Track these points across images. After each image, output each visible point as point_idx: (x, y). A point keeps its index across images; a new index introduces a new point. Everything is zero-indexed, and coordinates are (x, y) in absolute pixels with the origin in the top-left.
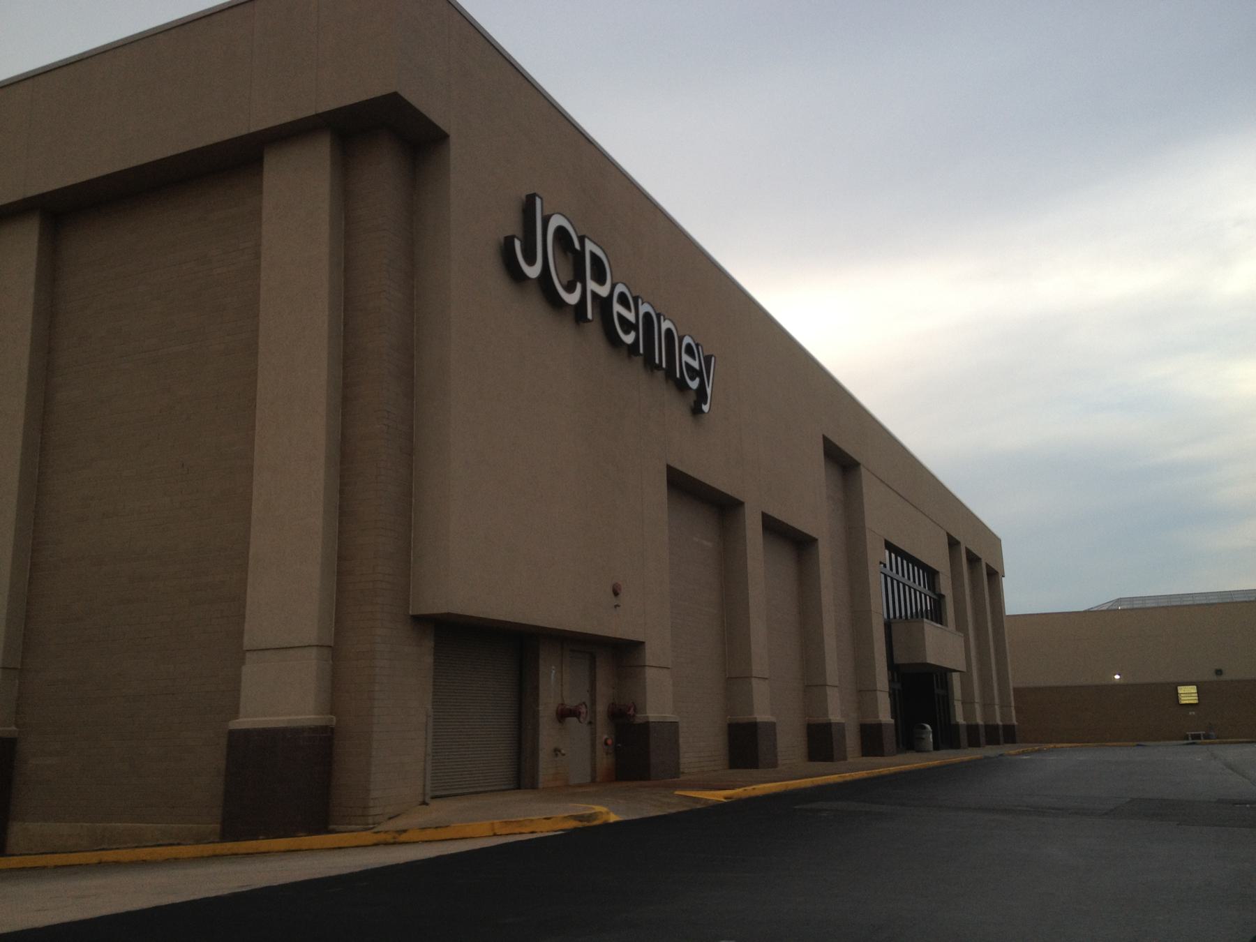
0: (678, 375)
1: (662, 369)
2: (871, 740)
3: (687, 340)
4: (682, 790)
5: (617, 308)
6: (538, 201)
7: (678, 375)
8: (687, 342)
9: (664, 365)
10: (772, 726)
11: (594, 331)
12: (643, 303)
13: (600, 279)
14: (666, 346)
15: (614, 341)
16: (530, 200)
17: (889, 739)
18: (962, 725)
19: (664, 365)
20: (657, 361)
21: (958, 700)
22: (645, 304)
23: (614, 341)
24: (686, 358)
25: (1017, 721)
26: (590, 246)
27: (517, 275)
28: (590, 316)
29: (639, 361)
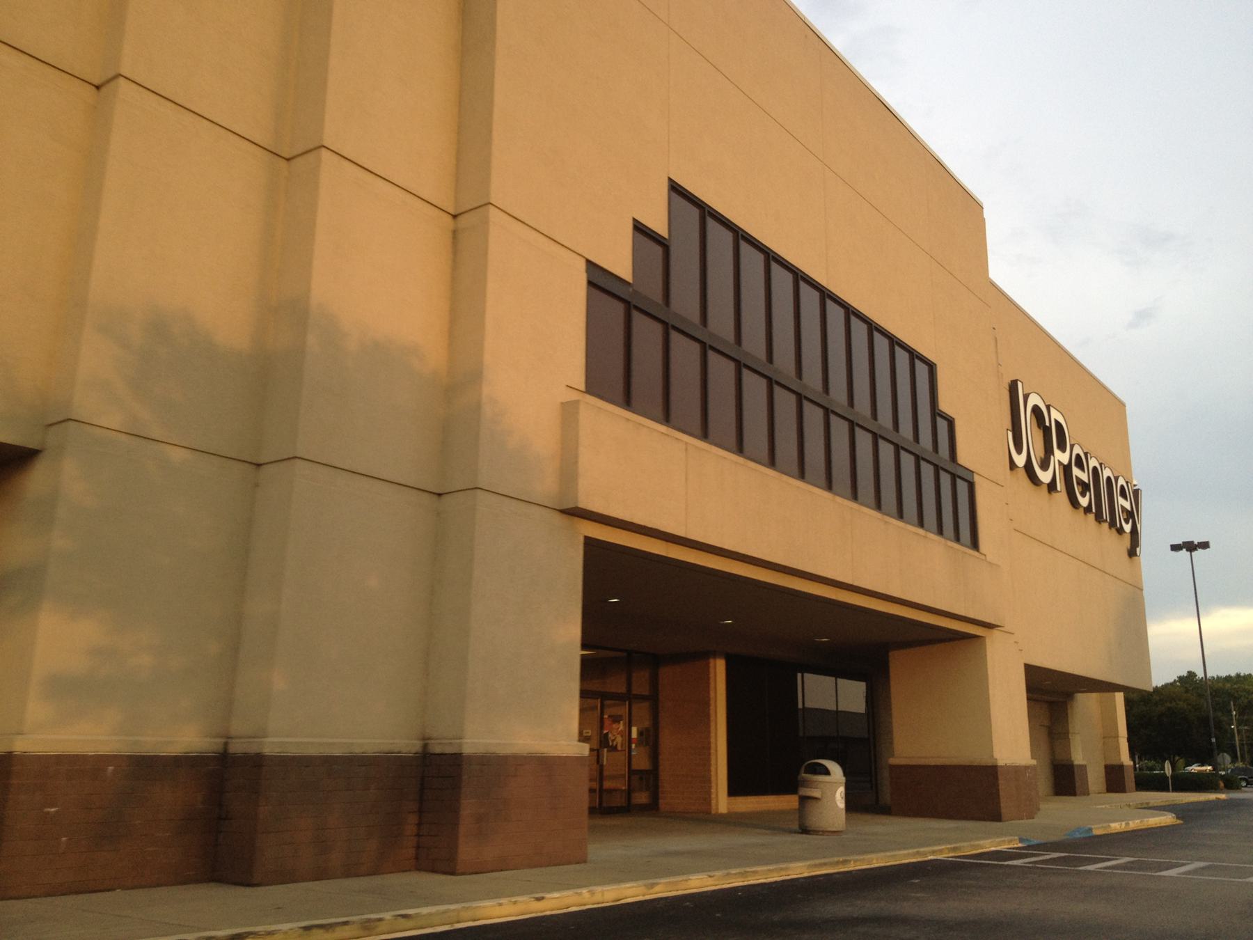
0: (1118, 526)
1: (1093, 513)
2: (1115, 780)
3: (1121, 481)
4: (1192, 803)
5: (1076, 471)
6: (1020, 384)
7: (1118, 526)
8: (1077, 453)
9: (1108, 520)
10: (1083, 767)
11: (1061, 496)
12: (1091, 457)
13: (1062, 447)
14: (1108, 494)
15: (1074, 503)
16: (1013, 387)
17: (1130, 779)
18: (1127, 766)
19: (1108, 520)
20: (1105, 518)
21: (1123, 737)
22: (1093, 458)
23: (1074, 503)
24: (1121, 501)
25: (1132, 756)
26: (1055, 415)
27: (1012, 465)
28: (1059, 489)
29: (1091, 517)
